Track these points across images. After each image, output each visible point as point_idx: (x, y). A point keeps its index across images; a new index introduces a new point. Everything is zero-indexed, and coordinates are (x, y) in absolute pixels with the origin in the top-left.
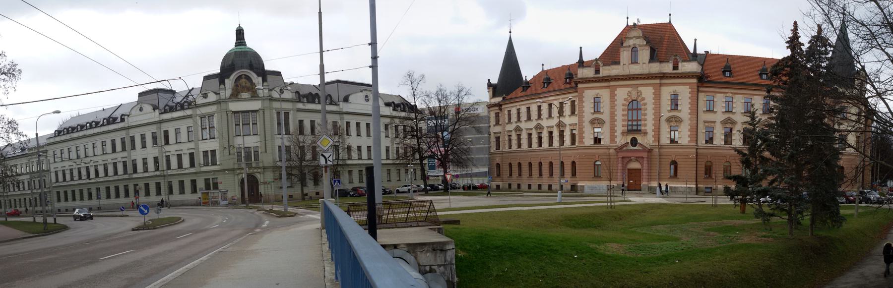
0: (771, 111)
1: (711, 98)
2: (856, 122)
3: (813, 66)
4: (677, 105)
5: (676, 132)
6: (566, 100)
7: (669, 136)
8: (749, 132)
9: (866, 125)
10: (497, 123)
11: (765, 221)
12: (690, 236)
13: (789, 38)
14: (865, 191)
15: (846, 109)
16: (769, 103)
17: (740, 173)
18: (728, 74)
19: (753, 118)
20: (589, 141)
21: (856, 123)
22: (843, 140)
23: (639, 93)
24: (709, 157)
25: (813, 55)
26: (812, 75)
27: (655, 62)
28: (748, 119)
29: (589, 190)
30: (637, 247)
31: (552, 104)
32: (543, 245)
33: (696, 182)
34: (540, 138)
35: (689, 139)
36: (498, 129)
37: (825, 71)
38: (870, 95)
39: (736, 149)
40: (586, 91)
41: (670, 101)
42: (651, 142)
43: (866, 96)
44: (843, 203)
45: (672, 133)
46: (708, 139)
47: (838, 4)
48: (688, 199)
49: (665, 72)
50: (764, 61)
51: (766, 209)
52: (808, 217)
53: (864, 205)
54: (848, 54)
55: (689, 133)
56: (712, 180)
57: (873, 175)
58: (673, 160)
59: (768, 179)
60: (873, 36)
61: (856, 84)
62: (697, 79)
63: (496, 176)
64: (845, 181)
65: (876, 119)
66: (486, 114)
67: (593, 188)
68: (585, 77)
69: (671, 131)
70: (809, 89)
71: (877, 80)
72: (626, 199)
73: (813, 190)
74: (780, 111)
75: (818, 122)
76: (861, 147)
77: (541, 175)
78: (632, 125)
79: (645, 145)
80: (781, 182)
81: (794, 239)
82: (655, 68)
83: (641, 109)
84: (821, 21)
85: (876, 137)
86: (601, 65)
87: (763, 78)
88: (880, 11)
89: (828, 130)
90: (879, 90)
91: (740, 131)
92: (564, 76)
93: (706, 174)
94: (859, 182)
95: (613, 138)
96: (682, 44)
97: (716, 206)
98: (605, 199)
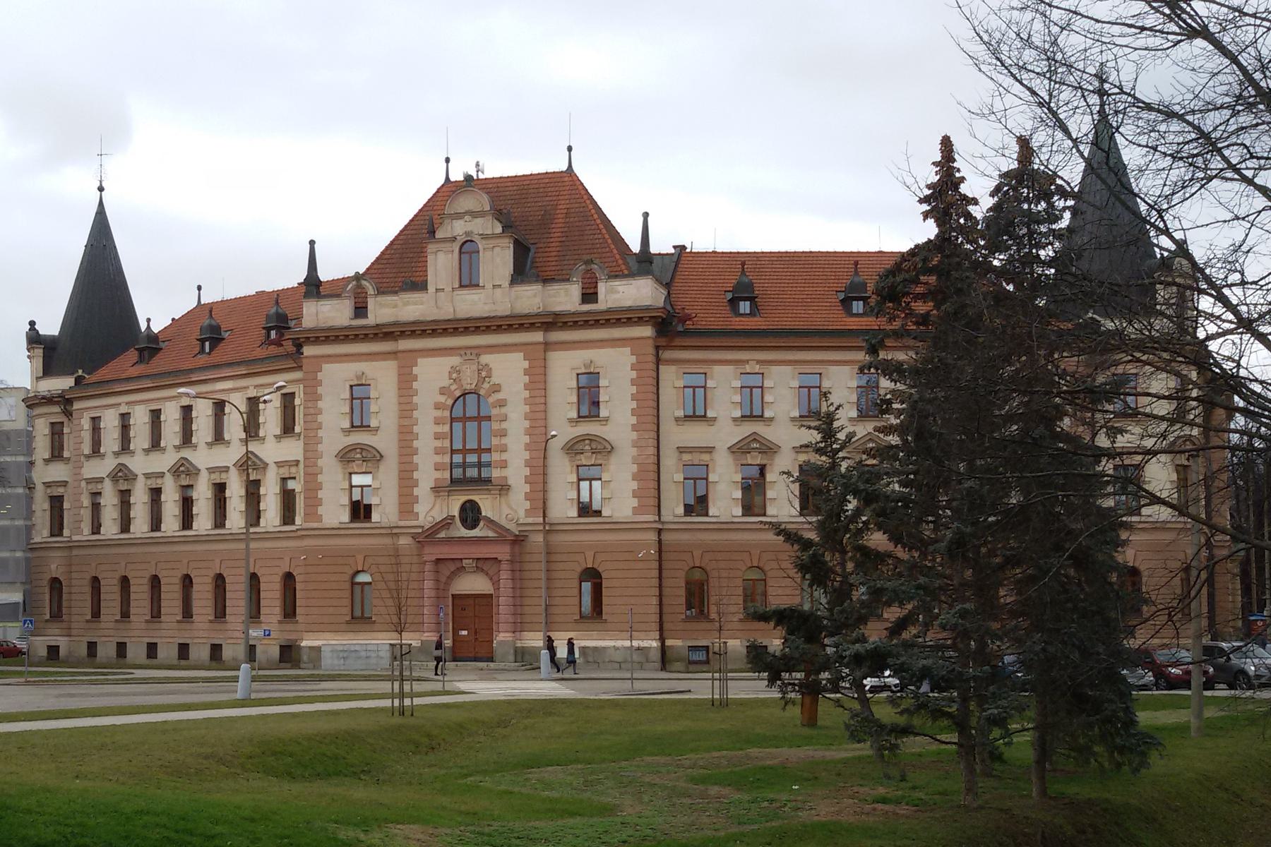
0: (883, 407)
1: (699, 380)
2: (1172, 422)
3: (1010, 261)
4: (596, 404)
5: (596, 484)
6: (267, 391)
7: (575, 497)
8: (820, 476)
9: (1207, 428)
10: (56, 454)
11: (881, 749)
12: (646, 798)
13: (929, 187)
14: (1224, 645)
15: (1132, 384)
16: (878, 383)
17: (797, 600)
18: (745, 307)
19: (828, 432)
20: (335, 513)
21: (1171, 425)
22: (1128, 481)
23: (484, 373)
24: (697, 553)
25: (1009, 228)
26: (1010, 288)
27: (530, 283)
28: (814, 436)
29: (336, 662)
30: (483, 834)
31: (224, 401)
32: (192, 834)
33: (661, 630)
34: (187, 504)
35: (635, 503)
36: (58, 472)
37: (1053, 271)
38: (1212, 329)
39: (778, 529)
40: (326, 367)
41: (575, 392)
42: (522, 513)
43: (1201, 334)
44: (1144, 687)
45: (585, 485)
46: (692, 502)
47: (1081, 67)
48: (639, 685)
49: (558, 308)
50: (855, 260)
51: (885, 713)
52: (1027, 737)
53: (1222, 692)
54: (1126, 213)
55: (634, 485)
56: (704, 625)
57: (1246, 590)
58: (590, 566)
59: (885, 615)
60: (1210, 143)
61: (1160, 299)
62: (654, 326)
63: (48, 617)
64: (1146, 615)
65: (1241, 404)
66: (21, 424)
67: (346, 654)
68: (322, 325)
69: (579, 480)
70: (1004, 332)
71: (1235, 277)
72: (448, 687)
73: (1038, 648)
74: (913, 406)
75: (1039, 431)
76: (1197, 500)
77: (187, 613)
78: (464, 465)
79: (503, 522)
80: (927, 626)
81: (981, 808)
82: (531, 298)
83: (489, 418)
84: (1029, 125)
85: (1248, 465)
86: (371, 291)
87: (855, 311)
88: (1227, 61)
89: (1075, 454)
90: (1244, 309)
91: (788, 473)
92: (263, 323)
93: (689, 607)
94: (1198, 616)
95: (407, 502)
96: (606, 227)
97: (724, 704)
98: (385, 687)
